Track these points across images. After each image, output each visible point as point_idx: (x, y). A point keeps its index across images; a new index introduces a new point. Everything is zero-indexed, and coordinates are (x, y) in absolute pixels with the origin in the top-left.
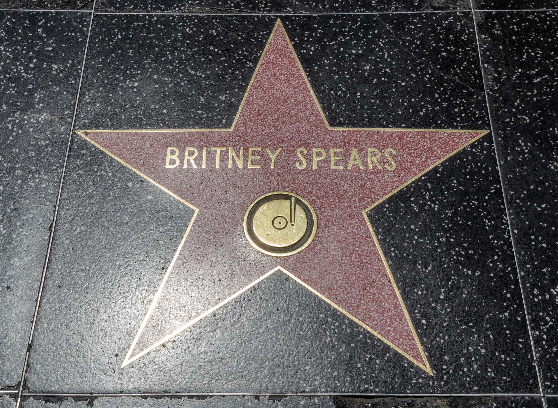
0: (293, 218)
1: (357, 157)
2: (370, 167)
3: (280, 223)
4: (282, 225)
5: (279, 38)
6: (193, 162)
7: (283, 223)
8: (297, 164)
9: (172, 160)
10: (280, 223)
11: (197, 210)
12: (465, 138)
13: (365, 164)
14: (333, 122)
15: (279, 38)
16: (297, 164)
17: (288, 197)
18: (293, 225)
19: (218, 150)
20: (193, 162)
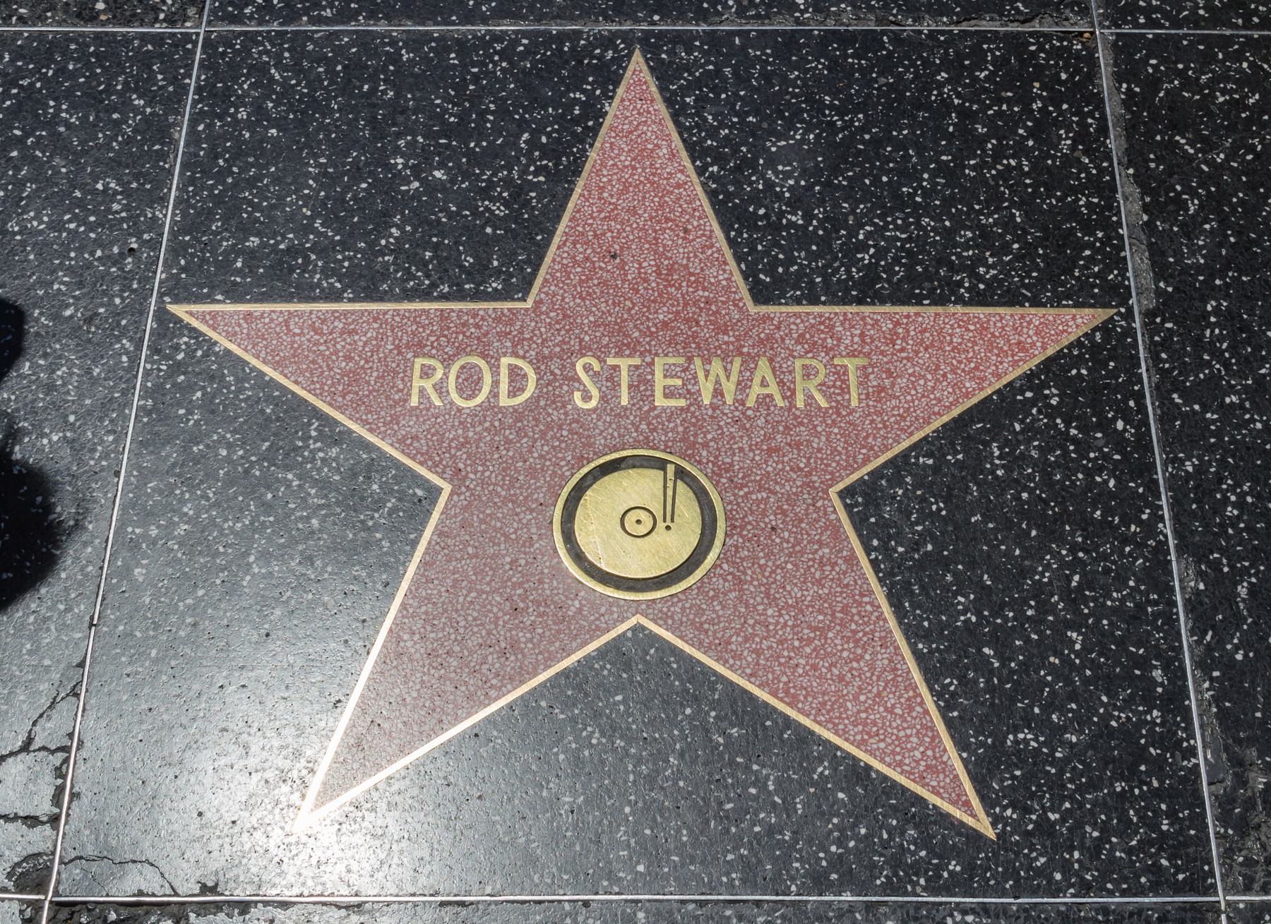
0: (670, 515)
1: (770, 378)
2: (800, 404)
3: (639, 522)
4: (643, 530)
5: (638, 123)
6: (430, 391)
7: (648, 523)
8: (577, 396)
9: (431, 384)
10: (639, 522)
11: (447, 488)
12: (1076, 322)
13: (790, 395)
14: (761, 294)
15: (638, 123)
16: (577, 396)
17: (661, 465)
18: (668, 528)
19: (624, 363)
20: (430, 391)
